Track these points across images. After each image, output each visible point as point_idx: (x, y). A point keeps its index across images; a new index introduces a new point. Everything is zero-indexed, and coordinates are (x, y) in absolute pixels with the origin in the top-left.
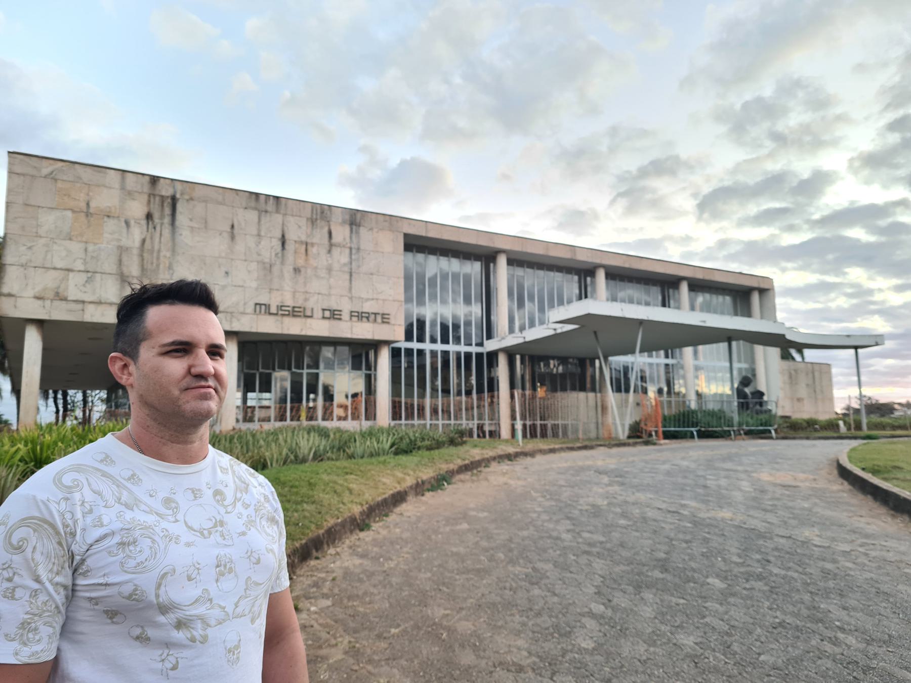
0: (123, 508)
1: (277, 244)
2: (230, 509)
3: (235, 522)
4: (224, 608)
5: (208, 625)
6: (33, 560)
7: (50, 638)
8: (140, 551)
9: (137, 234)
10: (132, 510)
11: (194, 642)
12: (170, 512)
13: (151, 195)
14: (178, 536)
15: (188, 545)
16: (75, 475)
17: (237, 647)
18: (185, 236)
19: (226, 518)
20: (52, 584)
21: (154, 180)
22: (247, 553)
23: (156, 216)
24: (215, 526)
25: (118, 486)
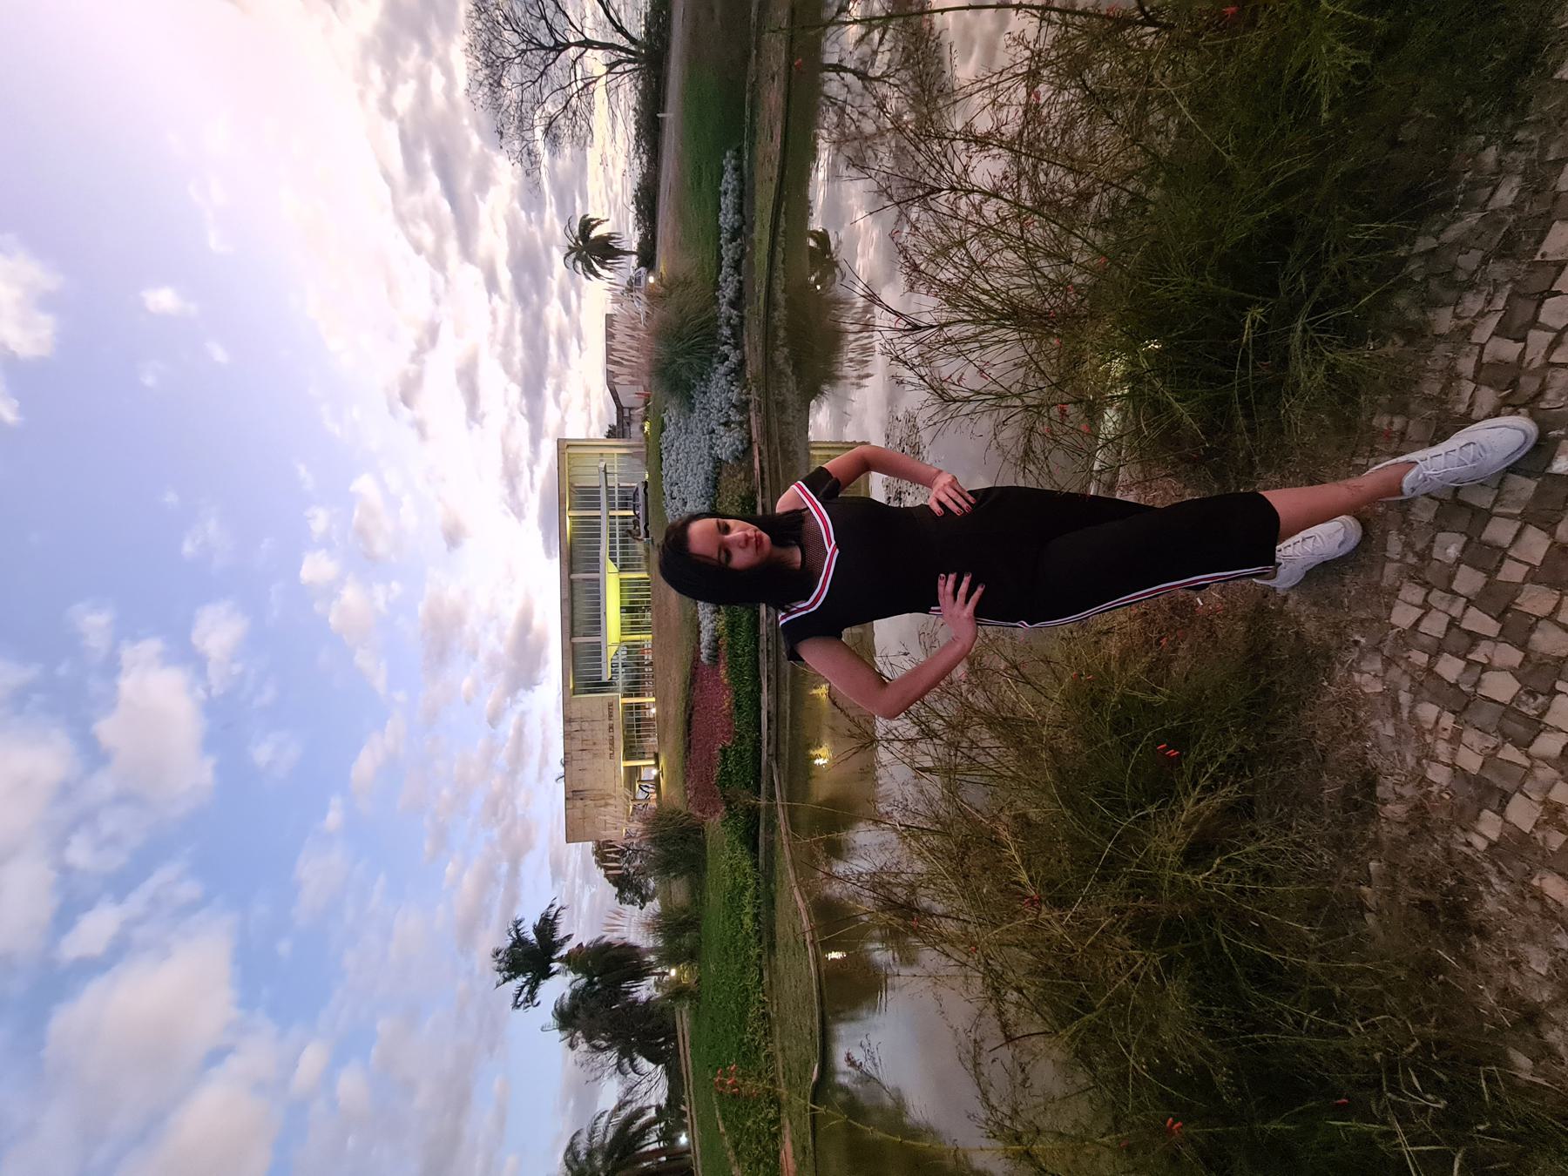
18: (587, 786)
21: (567, 799)
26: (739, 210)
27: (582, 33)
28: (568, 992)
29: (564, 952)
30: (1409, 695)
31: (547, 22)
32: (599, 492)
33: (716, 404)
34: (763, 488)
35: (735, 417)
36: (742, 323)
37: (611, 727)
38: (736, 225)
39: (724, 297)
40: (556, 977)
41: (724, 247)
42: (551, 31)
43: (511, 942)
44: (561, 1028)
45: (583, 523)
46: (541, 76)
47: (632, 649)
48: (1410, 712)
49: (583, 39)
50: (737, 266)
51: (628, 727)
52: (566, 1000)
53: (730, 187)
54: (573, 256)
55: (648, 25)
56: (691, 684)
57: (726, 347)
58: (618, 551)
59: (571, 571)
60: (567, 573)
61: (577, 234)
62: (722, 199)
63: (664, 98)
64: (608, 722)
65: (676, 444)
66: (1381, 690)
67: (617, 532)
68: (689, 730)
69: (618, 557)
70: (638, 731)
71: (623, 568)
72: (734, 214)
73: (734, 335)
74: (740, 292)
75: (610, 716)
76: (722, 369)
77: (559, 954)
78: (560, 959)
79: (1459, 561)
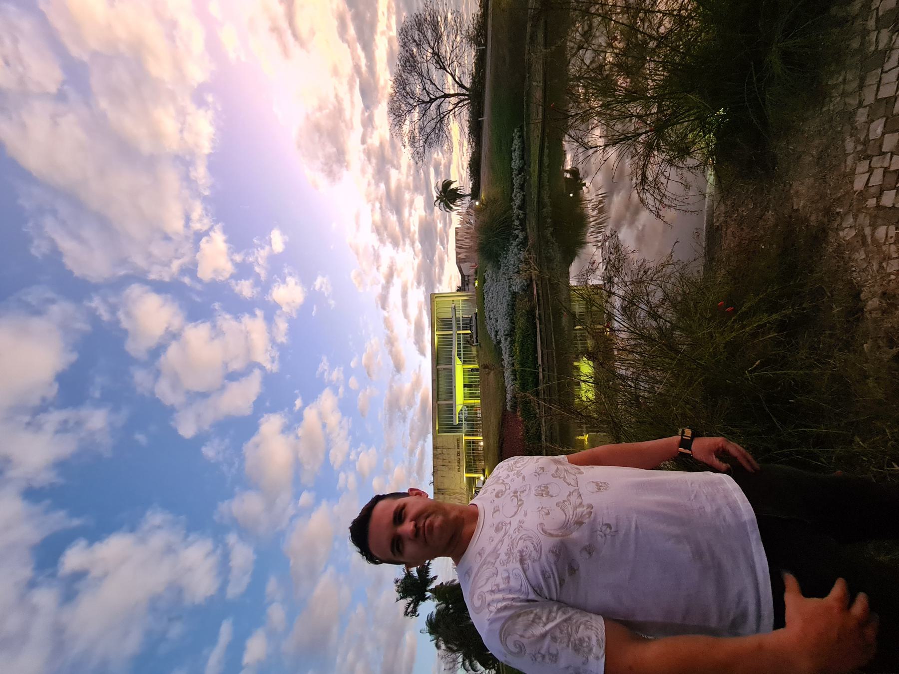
0: (498, 561)
1: (444, 467)
2: (508, 487)
3: (517, 484)
4: (570, 492)
5: (581, 503)
6: (529, 638)
7: (588, 628)
8: (527, 548)
9: (446, 496)
10: (499, 554)
11: (591, 512)
12: (504, 527)
13: (438, 493)
14: (520, 522)
15: (526, 514)
16: (475, 597)
17: (597, 484)
18: (446, 487)
19: (512, 489)
20: (548, 623)
21: (434, 493)
22: (536, 476)
23: (442, 492)
24: (517, 497)
25: (484, 564)
26: (522, 157)
27: (443, 92)
28: (435, 611)
29: (433, 586)
30: (869, 228)
31: (426, 90)
32: (451, 321)
33: (512, 262)
34: (539, 305)
35: (522, 266)
36: (525, 217)
37: (459, 453)
38: (521, 166)
39: (515, 205)
40: (428, 601)
41: (515, 179)
42: (428, 94)
43: (404, 576)
44: (431, 633)
45: (444, 338)
46: (423, 116)
47: (470, 408)
48: (872, 237)
49: (443, 94)
50: (522, 187)
51: (468, 454)
52: (434, 616)
53: (517, 147)
54: (439, 201)
55: (474, 78)
56: (502, 425)
57: (516, 231)
58: (462, 353)
59: (438, 364)
60: (435, 365)
61: (441, 189)
62: (513, 154)
63: (482, 112)
64: (457, 450)
65: (492, 288)
66: (855, 233)
67: (462, 342)
68: (501, 452)
69: (462, 356)
70: (473, 457)
71: (465, 362)
72: (519, 160)
73: (521, 224)
74: (524, 201)
75: (458, 446)
76: (515, 243)
77: (431, 587)
78: (431, 591)
79: (883, 134)
